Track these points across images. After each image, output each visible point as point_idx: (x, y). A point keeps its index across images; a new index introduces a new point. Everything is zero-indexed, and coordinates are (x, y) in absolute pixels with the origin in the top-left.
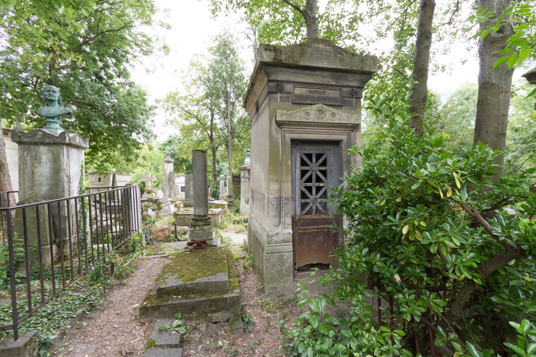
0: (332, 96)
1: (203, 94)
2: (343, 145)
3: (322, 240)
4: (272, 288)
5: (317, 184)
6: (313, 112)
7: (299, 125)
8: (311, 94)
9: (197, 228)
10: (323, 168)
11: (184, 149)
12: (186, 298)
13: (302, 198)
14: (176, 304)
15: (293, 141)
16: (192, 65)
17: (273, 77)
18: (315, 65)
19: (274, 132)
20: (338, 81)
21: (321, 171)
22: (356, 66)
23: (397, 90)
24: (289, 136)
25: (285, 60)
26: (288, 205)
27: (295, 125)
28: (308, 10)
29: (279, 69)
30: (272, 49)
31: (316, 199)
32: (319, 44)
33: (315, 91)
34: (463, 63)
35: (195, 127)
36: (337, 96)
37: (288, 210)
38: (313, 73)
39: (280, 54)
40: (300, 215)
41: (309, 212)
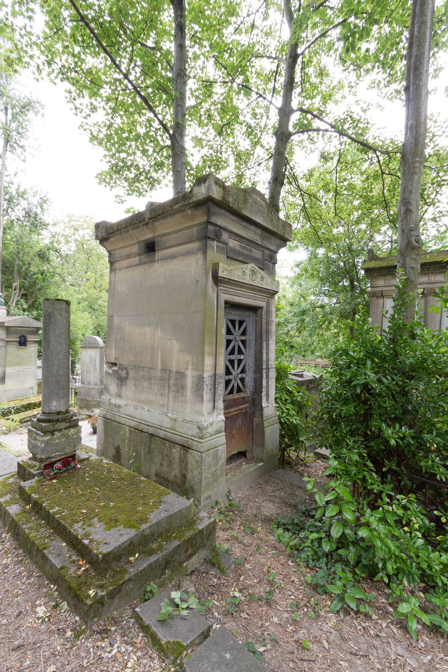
3: (241, 423)
4: (207, 499)
8: (242, 250)
9: (57, 434)
12: (151, 553)
14: (144, 569)
15: (226, 303)
17: (214, 219)
24: (224, 297)
27: (231, 284)
29: (223, 211)
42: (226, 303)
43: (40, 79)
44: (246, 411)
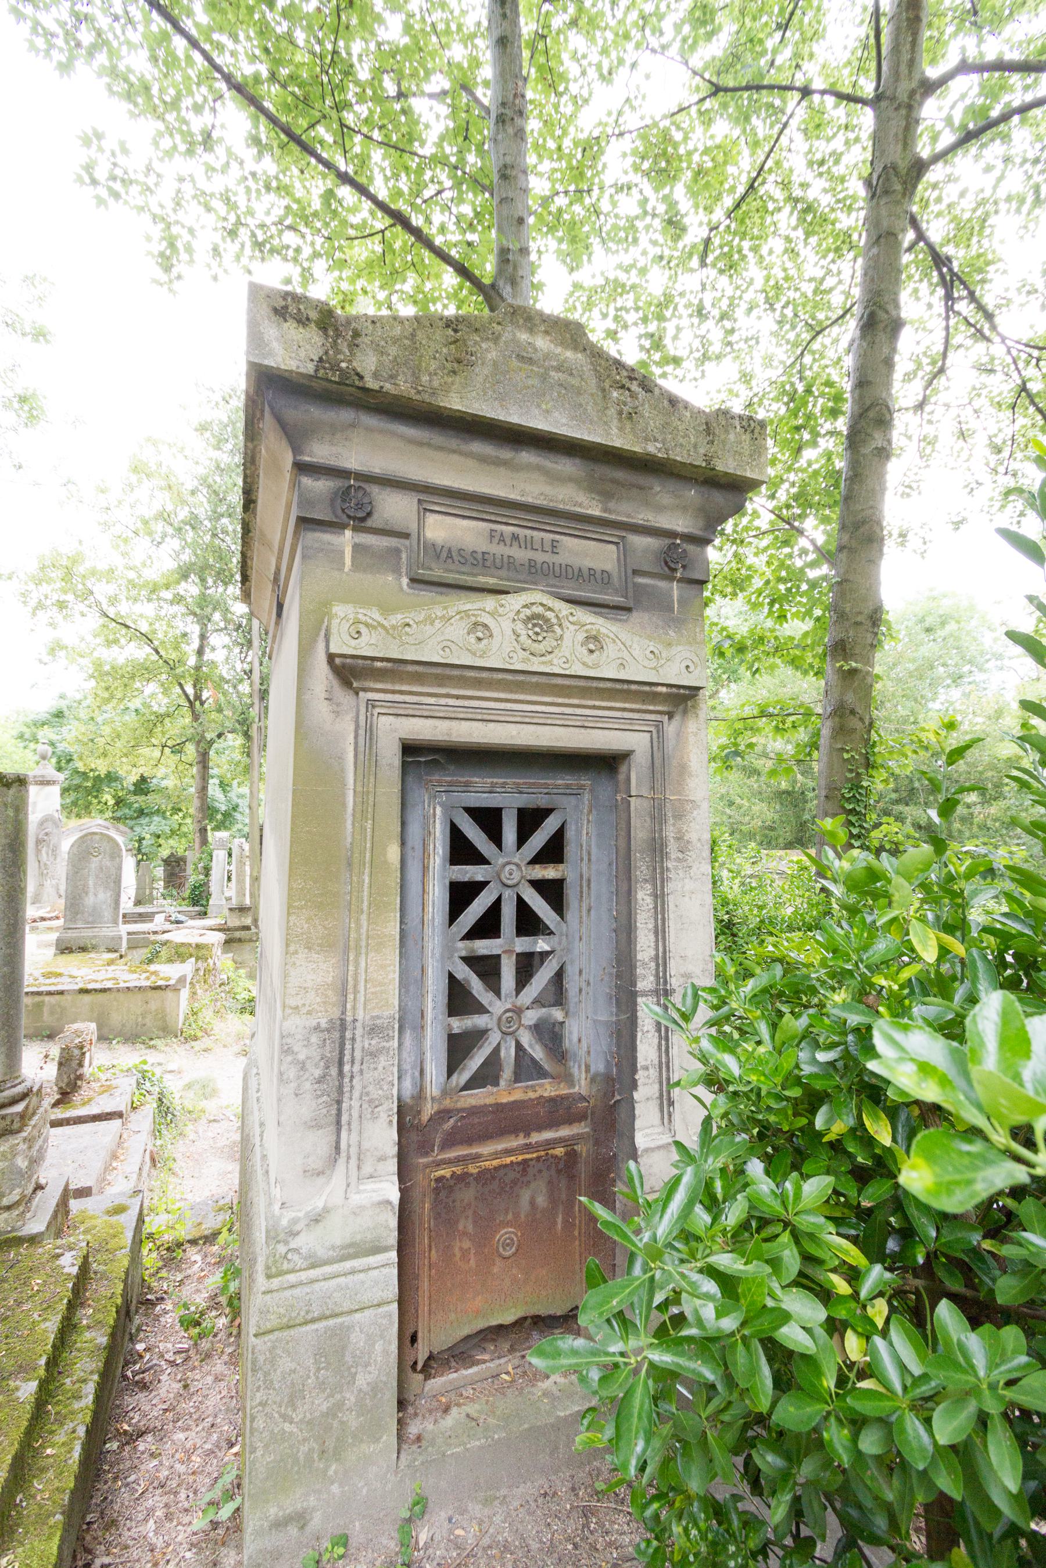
0: (587, 563)
1: (172, 565)
2: (636, 774)
3: (541, 1201)
4: (279, 1524)
5: (522, 944)
6: (507, 625)
7: (441, 680)
10: (549, 872)
11: (101, 741)
13: (521, 812)
15: (410, 749)
16: (135, 470)
17: (320, 452)
18: (514, 416)
19: (320, 709)
20: (611, 505)
21: (539, 885)
22: (687, 451)
23: (782, 587)
24: (394, 730)
25: (376, 375)
26: (383, 1061)
27: (418, 678)
28: (501, 283)
29: (346, 415)
30: (314, 315)
31: (518, 1011)
32: (531, 331)
33: (515, 537)
34: (957, 525)
35: (144, 671)
36: (608, 567)
37: (378, 1083)
38: (506, 454)
39: (353, 346)
40: (445, 1093)
41: (488, 1075)
42: (410, 749)
43: (220, 273)
44: (572, 1156)
